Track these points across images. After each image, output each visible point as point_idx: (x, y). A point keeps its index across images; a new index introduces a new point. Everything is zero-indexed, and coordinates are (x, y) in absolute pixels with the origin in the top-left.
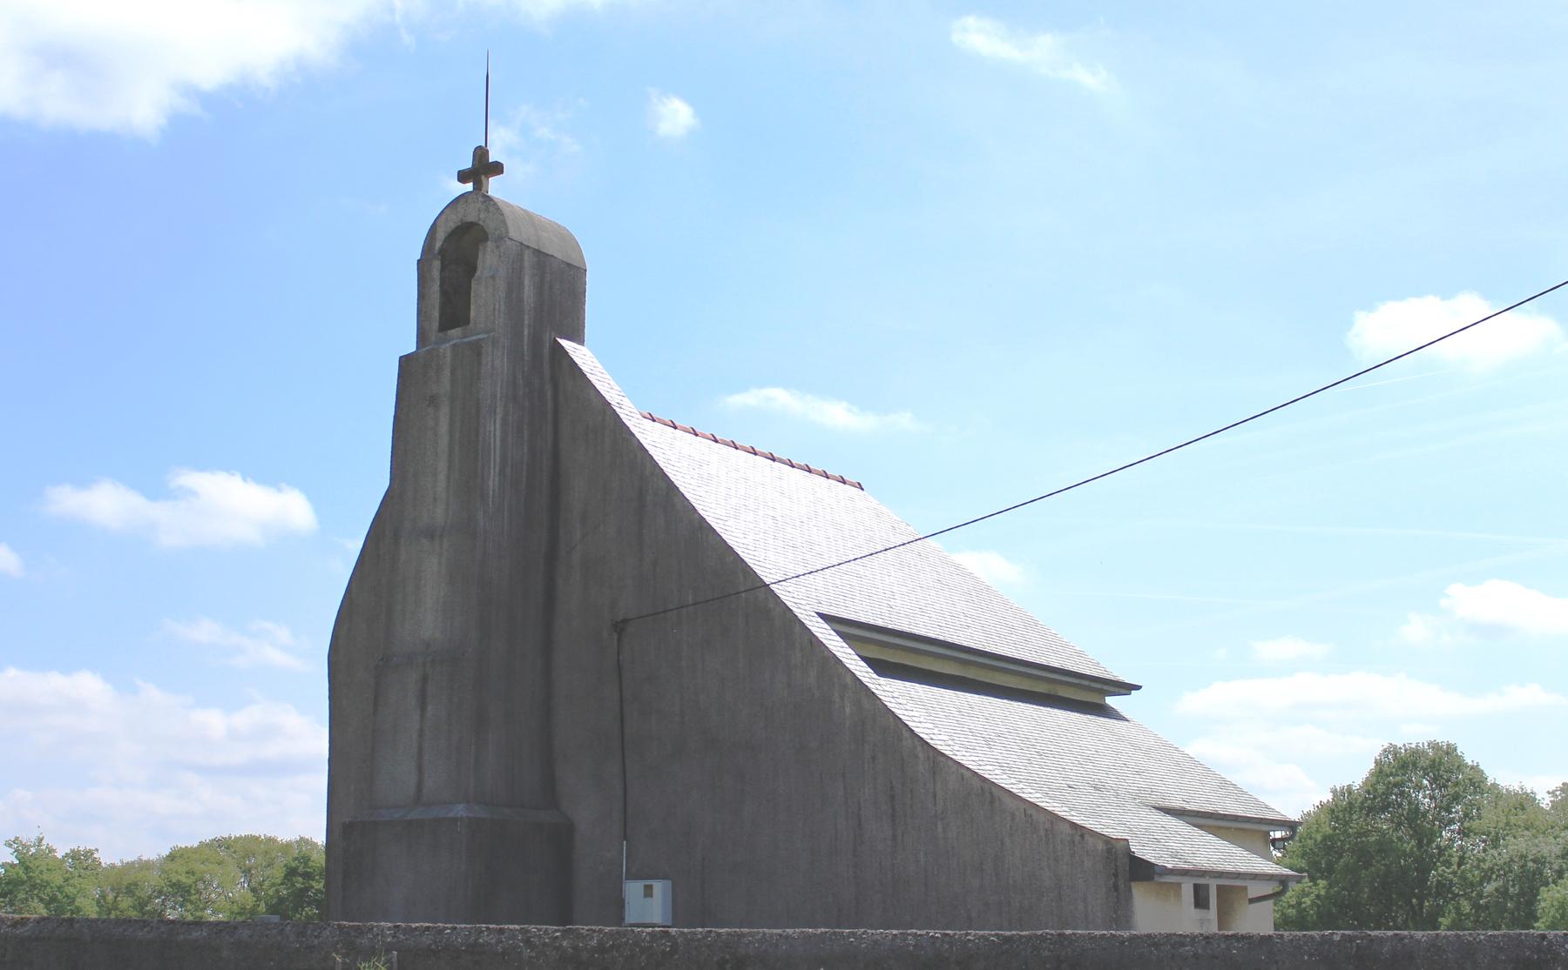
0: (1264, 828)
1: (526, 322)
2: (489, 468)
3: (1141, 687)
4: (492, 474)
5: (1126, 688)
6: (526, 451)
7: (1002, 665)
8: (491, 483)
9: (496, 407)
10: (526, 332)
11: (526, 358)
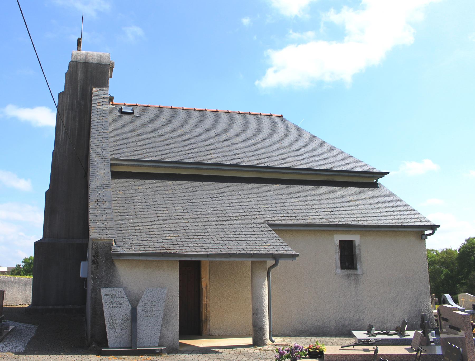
0: (422, 230)
1: (79, 85)
2: (60, 133)
3: (389, 173)
4: (61, 134)
5: (383, 174)
6: (77, 124)
7: (310, 172)
8: (60, 137)
9: (63, 113)
10: (79, 88)
11: (79, 96)
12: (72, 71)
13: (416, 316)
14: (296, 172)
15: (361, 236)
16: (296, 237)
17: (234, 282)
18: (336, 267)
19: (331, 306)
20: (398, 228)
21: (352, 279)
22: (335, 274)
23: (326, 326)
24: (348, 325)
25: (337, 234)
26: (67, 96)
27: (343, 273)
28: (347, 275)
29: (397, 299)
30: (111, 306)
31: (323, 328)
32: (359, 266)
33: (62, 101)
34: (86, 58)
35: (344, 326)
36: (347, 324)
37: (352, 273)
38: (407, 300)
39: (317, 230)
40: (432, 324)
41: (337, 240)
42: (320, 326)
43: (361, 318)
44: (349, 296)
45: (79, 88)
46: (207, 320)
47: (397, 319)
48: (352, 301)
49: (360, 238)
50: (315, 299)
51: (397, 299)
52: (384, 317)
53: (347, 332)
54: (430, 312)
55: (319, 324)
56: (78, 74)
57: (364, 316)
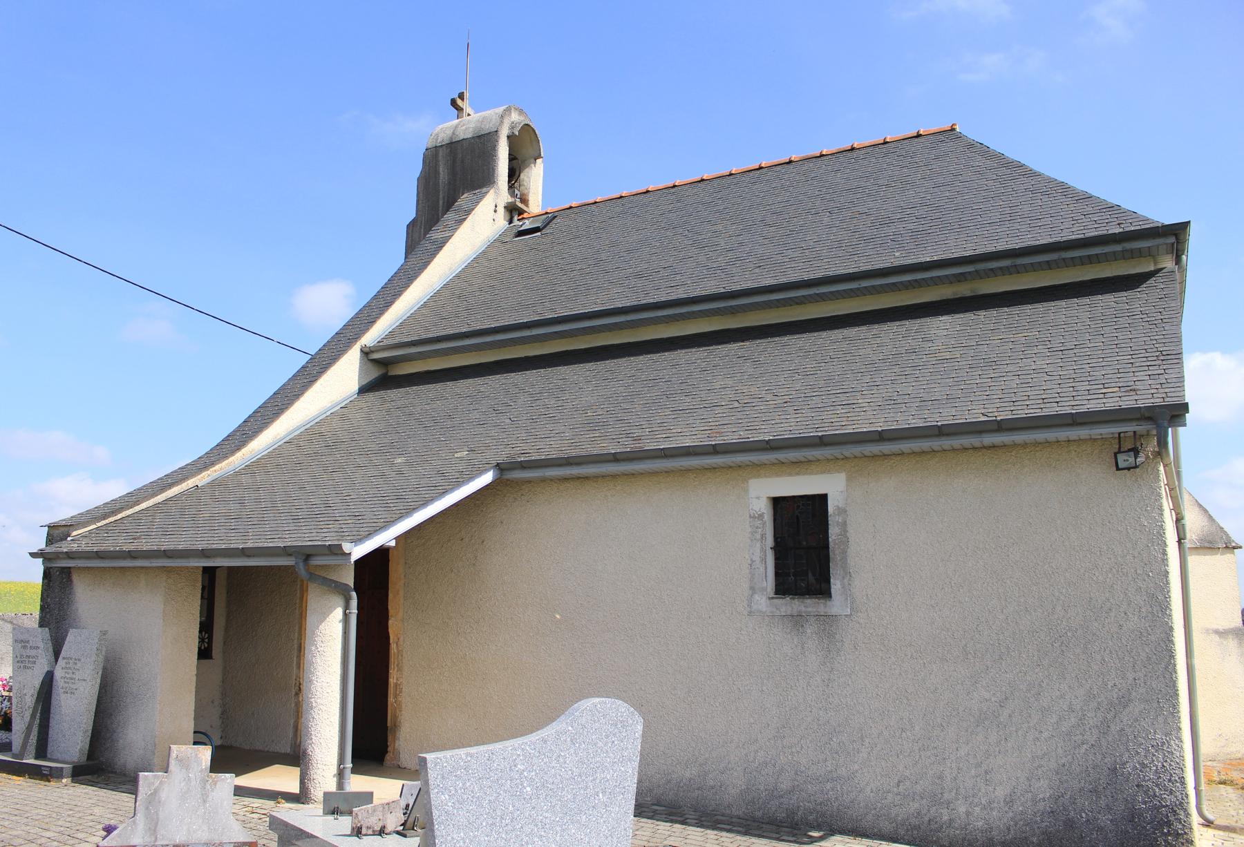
1: (441, 196)
10: (441, 202)
12: (429, 170)
13: (1094, 791)
14: (818, 292)
15: (849, 479)
16: (625, 495)
17: (457, 631)
18: (752, 588)
19: (730, 718)
20: (980, 432)
21: (809, 631)
22: (745, 613)
23: (712, 783)
24: (791, 791)
25: (759, 476)
26: (421, 227)
27: (775, 610)
28: (792, 616)
29: (1006, 713)
30: (22, 665)
31: (698, 789)
32: (836, 585)
33: (412, 240)
34: (453, 133)
35: (775, 793)
36: (785, 785)
37: (810, 609)
38: (1054, 719)
39: (688, 470)
40: (1169, 833)
41: (758, 498)
42: (690, 780)
43: (843, 771)
44: (800, 689)
45: (441, 202)
46: (396, 726)
47: (1001, 793)
48: (809, 709)
49: (847, 485)
50: (679, 693)
51: (1006, 713)
52: (940, 778)
53: (784, 815)
54: (1170, 780)
55: (688, 775)
56: (439, 174)
57: (856, 767)
